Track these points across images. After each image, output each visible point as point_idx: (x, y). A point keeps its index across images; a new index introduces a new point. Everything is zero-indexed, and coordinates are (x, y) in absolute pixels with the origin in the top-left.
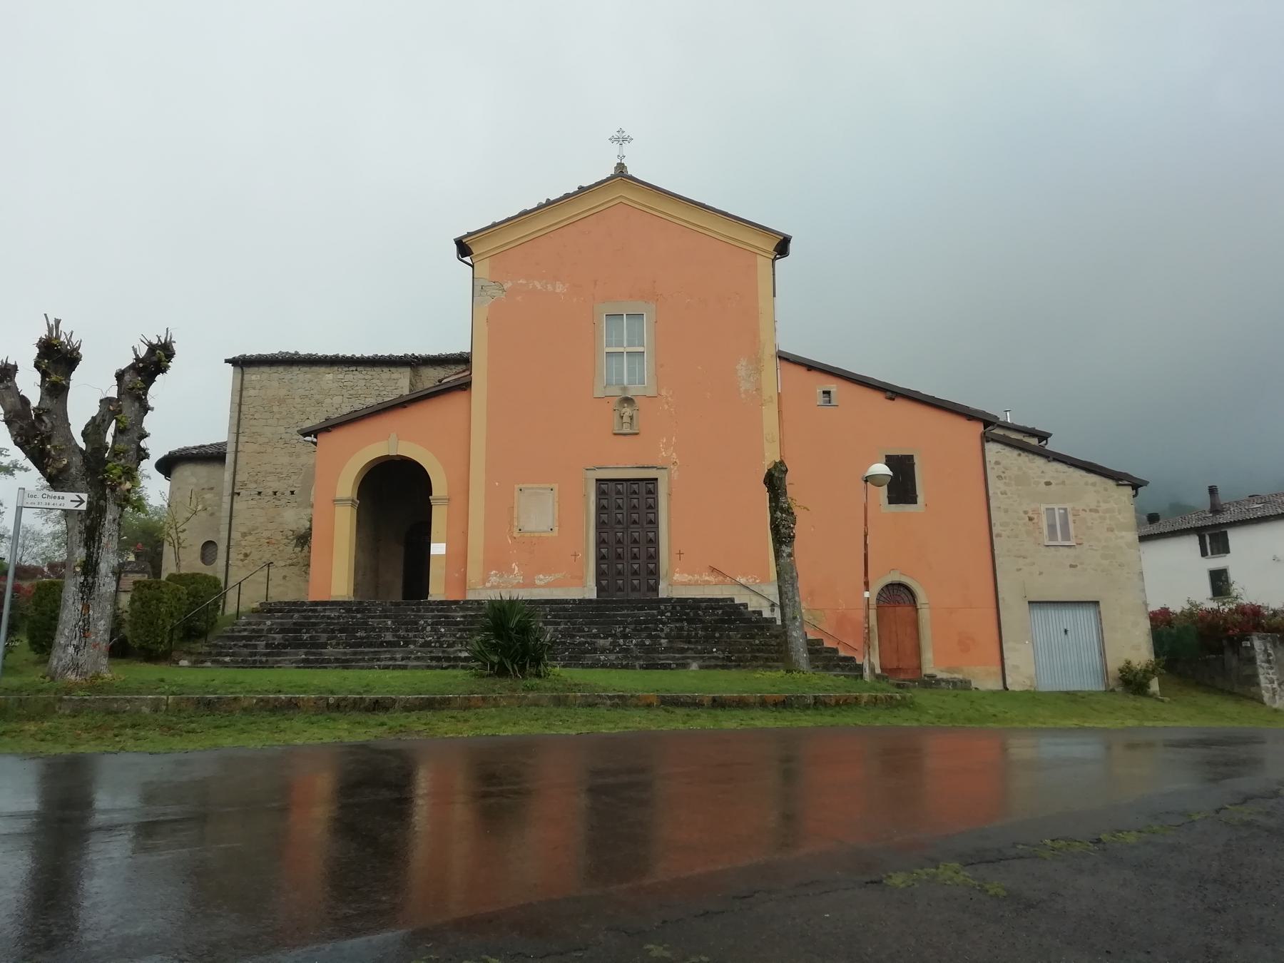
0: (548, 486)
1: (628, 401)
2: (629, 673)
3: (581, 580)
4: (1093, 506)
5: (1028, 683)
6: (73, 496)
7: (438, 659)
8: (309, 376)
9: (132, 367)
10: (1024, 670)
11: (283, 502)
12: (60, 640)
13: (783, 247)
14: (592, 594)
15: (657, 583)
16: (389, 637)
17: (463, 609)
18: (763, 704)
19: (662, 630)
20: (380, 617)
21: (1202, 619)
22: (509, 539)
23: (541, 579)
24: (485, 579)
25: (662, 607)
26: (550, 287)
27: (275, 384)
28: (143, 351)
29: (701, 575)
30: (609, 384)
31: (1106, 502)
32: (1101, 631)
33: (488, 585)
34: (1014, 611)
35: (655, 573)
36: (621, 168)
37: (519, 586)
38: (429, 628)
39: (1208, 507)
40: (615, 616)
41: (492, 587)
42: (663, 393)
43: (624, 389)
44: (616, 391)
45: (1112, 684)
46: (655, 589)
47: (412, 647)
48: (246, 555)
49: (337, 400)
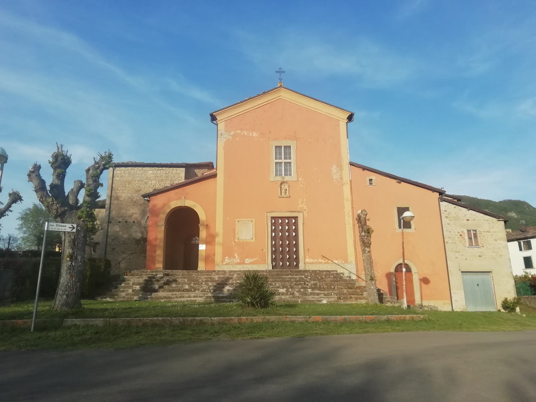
4: (488, 229)
5: (462, 308)
6: (70, 225)
9: (94, 166)
12: (104, 307)
16: (187, 287)
19: (308, 285)
20: (182, 278)
23: (247, 261)
24: (223, 261)
25: (306, 274)
27: (127, 175)
28: (98, 159)
31: (493, 228)
35: (297, 259)
38: (204, 283)
40: (285, 278)
41: (226, 264)
42: (300, 179)
47: (197, 291)
48: (114, 249)
49: (154, 182)
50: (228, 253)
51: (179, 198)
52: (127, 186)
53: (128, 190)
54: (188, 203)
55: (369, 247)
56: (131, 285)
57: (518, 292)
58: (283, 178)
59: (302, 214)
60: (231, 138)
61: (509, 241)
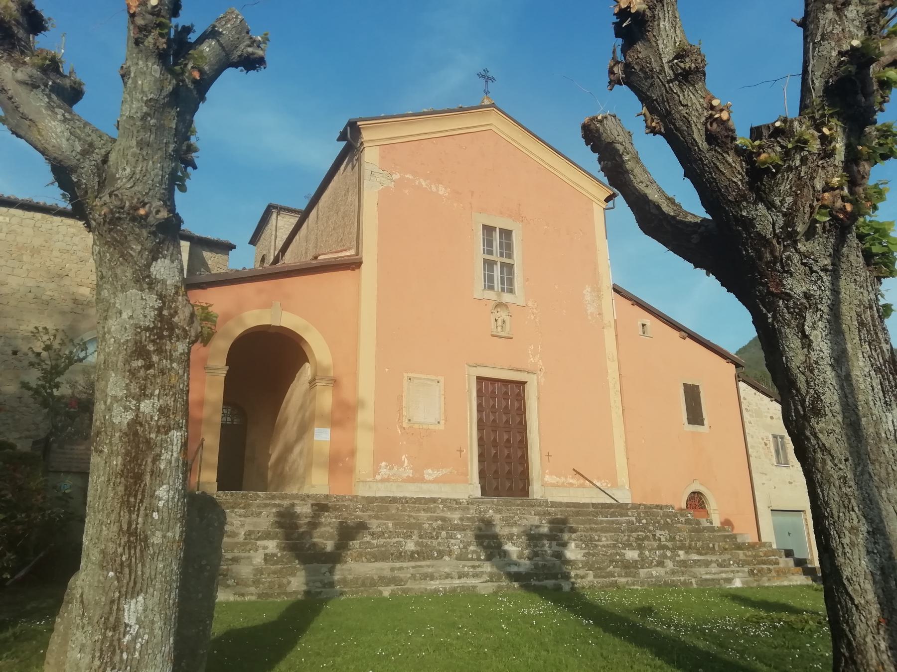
0: (434, 377)
24: (375, 472)
29: (566, 478)
33: (378, 477)
41: (383, 481)
47: (447, 558)
50: (386, 452)
51: (267, 305)
52: (25, 258)
53: (29, 271)
54: (288, 320)
56: (241, 538)
58: (499, 295)
59: (534, 377)
60: (392, 185)
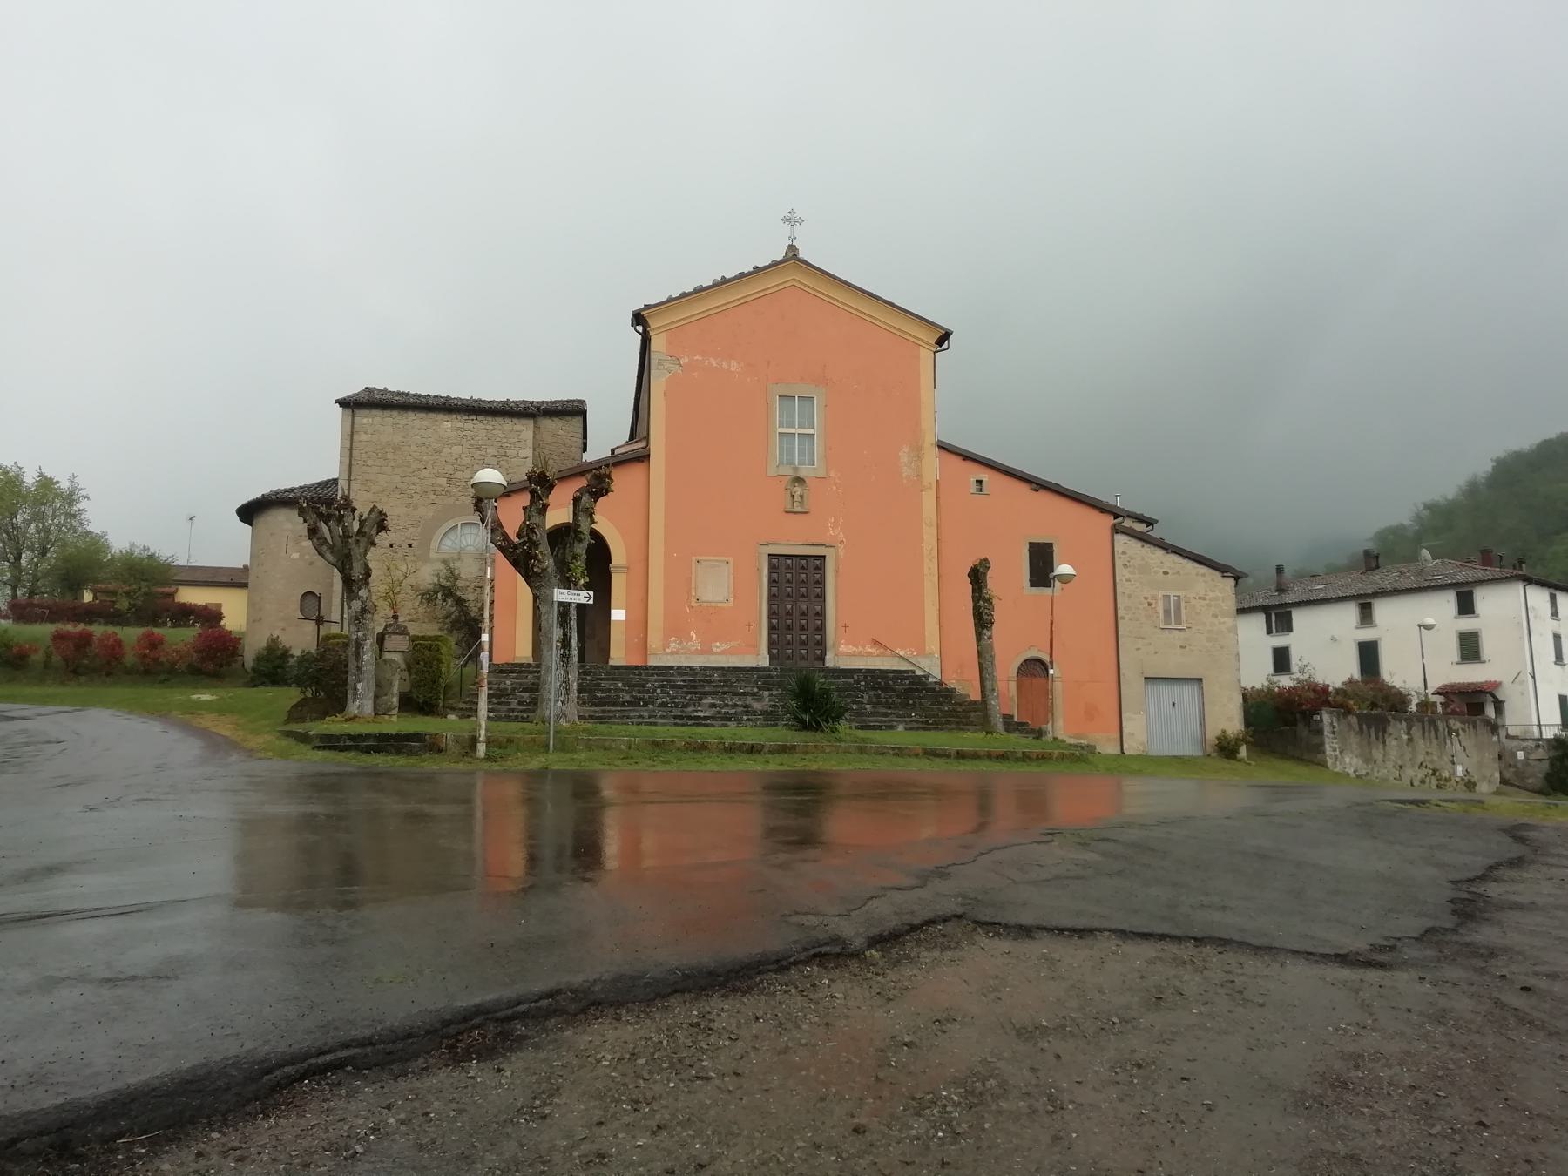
1: (799, 480)
2: (927, 733)
3: (754, 647)
4: (1202, 594)
7: (681, 718)
8: (425, 423)
10: (1140, 734)
11: (400, 555)
13: (944, 337)
14: (765, 662)
15: (824, 653)
16: (627, 698)
17: (680, 674)
18: (989, 756)
21: (1280, 694)
22: (687, 604)
23: (718, 646)
24: (665, 646)
26: (725, 365)
30: (781, 463)
32: (1202, 705)
34: (1133, 686)
35: (821, 644)
36: (792, 248)
37: (697, 652)
39: (1273, 587)
41: (672, 653)
43: (796, 469)
44: (788, 471)
45: (1209, 749)
46: (822, 658)
49: (457, 450)
55: (990, 628)
57: (1248, 722)
61: (1241, 611)
